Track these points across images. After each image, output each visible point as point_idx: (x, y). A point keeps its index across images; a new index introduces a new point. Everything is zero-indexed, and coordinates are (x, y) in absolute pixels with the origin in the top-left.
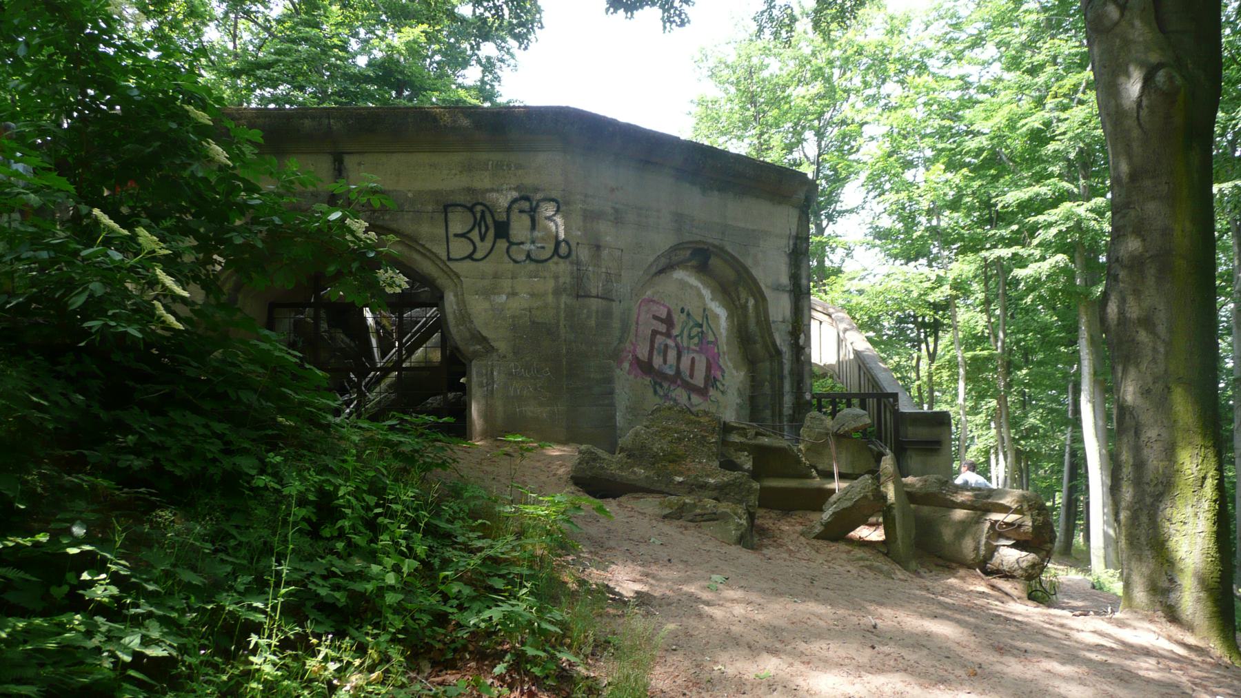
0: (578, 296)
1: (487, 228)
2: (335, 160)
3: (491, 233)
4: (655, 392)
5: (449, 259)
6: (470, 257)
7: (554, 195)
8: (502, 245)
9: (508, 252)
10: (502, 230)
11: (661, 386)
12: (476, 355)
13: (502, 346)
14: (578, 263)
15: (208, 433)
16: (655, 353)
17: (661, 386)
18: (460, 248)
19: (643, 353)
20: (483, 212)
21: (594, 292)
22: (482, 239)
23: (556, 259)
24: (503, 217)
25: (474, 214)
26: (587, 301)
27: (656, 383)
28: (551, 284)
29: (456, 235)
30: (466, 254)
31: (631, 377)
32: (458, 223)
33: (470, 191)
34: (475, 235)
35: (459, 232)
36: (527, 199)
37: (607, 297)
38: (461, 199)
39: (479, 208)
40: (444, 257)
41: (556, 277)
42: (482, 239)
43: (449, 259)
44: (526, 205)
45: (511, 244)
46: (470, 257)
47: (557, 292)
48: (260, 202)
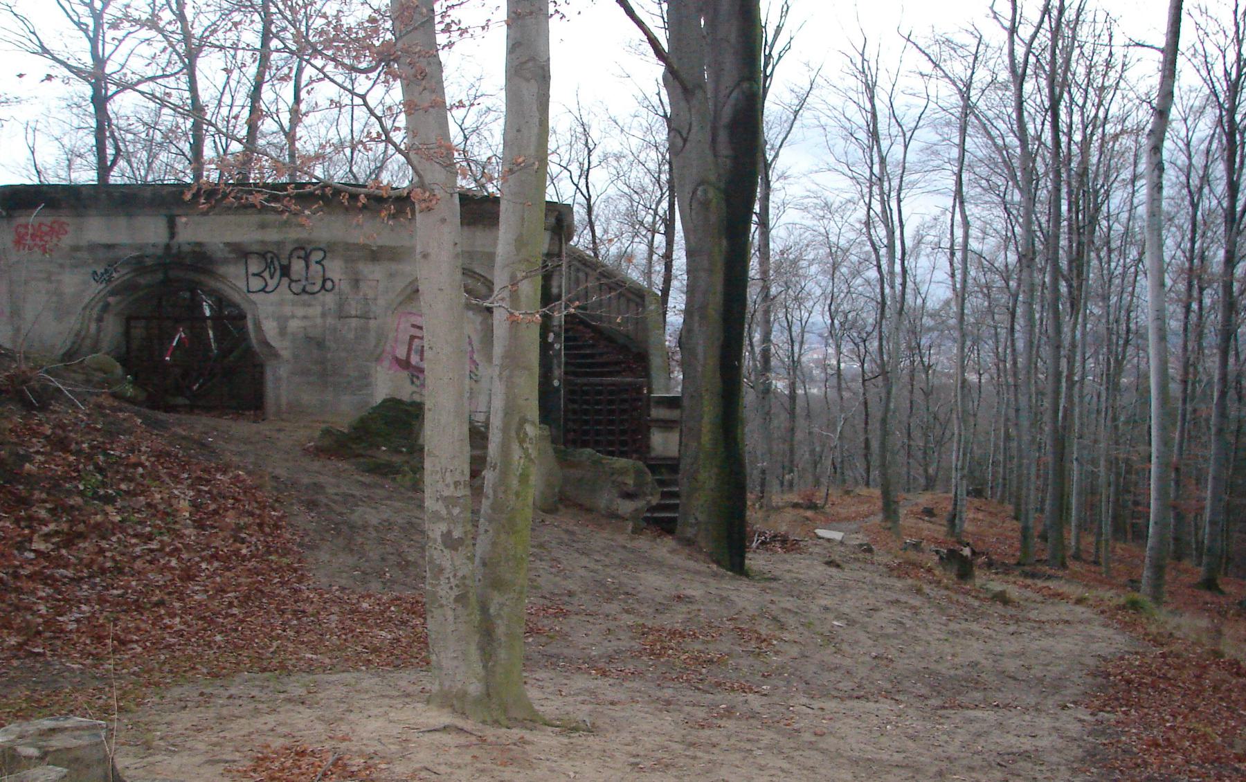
0: (340, 317)
1: (275, 270)
2: (168, 222)
3: (278, 273)
4: (413, 382)
5: (249, 291)
6: (263, 290)
7: (322, 246)
8: (285, 281)
9: (289, 287)
10: (285, 271)
11: (418, 378)
12: (954, 159)
13: (285, 354)
14: (340, 293)
15: (862, 357)
16: (413, 352)
17: (418, 378)
18: (256, 284)
19: (401, 353)
20: (272, 258)
21: (353, 313)
22: (272, 277)
23: (323, 291)
24: (285, 262)
25: (266, 260)
26: (348, 320)
27: (413, 375)
28: (319, 310)
29: (254, 275)
30: (261, 287)
31: (390, 372)
32: (254, 267)
33: (263, 242)
34: (266, 275)
35: (256, 272)
36: (303, 248)
37: (365, 316)
38: (255, 248)
39: (269, 255)
40: (245, 290)
41: (323, 306)
42: (272, 277)
43: (249, 291)
44: (302, 253)
45: (292, 281)
46: (263, 290)
47: (324, 315)
48: (86, 740)
